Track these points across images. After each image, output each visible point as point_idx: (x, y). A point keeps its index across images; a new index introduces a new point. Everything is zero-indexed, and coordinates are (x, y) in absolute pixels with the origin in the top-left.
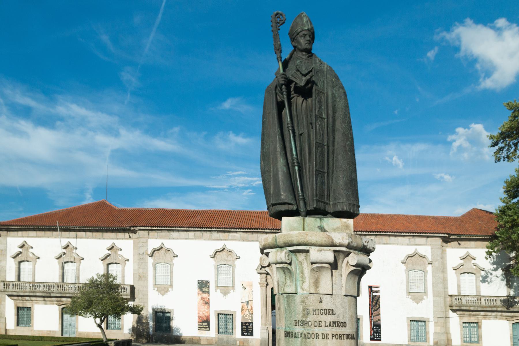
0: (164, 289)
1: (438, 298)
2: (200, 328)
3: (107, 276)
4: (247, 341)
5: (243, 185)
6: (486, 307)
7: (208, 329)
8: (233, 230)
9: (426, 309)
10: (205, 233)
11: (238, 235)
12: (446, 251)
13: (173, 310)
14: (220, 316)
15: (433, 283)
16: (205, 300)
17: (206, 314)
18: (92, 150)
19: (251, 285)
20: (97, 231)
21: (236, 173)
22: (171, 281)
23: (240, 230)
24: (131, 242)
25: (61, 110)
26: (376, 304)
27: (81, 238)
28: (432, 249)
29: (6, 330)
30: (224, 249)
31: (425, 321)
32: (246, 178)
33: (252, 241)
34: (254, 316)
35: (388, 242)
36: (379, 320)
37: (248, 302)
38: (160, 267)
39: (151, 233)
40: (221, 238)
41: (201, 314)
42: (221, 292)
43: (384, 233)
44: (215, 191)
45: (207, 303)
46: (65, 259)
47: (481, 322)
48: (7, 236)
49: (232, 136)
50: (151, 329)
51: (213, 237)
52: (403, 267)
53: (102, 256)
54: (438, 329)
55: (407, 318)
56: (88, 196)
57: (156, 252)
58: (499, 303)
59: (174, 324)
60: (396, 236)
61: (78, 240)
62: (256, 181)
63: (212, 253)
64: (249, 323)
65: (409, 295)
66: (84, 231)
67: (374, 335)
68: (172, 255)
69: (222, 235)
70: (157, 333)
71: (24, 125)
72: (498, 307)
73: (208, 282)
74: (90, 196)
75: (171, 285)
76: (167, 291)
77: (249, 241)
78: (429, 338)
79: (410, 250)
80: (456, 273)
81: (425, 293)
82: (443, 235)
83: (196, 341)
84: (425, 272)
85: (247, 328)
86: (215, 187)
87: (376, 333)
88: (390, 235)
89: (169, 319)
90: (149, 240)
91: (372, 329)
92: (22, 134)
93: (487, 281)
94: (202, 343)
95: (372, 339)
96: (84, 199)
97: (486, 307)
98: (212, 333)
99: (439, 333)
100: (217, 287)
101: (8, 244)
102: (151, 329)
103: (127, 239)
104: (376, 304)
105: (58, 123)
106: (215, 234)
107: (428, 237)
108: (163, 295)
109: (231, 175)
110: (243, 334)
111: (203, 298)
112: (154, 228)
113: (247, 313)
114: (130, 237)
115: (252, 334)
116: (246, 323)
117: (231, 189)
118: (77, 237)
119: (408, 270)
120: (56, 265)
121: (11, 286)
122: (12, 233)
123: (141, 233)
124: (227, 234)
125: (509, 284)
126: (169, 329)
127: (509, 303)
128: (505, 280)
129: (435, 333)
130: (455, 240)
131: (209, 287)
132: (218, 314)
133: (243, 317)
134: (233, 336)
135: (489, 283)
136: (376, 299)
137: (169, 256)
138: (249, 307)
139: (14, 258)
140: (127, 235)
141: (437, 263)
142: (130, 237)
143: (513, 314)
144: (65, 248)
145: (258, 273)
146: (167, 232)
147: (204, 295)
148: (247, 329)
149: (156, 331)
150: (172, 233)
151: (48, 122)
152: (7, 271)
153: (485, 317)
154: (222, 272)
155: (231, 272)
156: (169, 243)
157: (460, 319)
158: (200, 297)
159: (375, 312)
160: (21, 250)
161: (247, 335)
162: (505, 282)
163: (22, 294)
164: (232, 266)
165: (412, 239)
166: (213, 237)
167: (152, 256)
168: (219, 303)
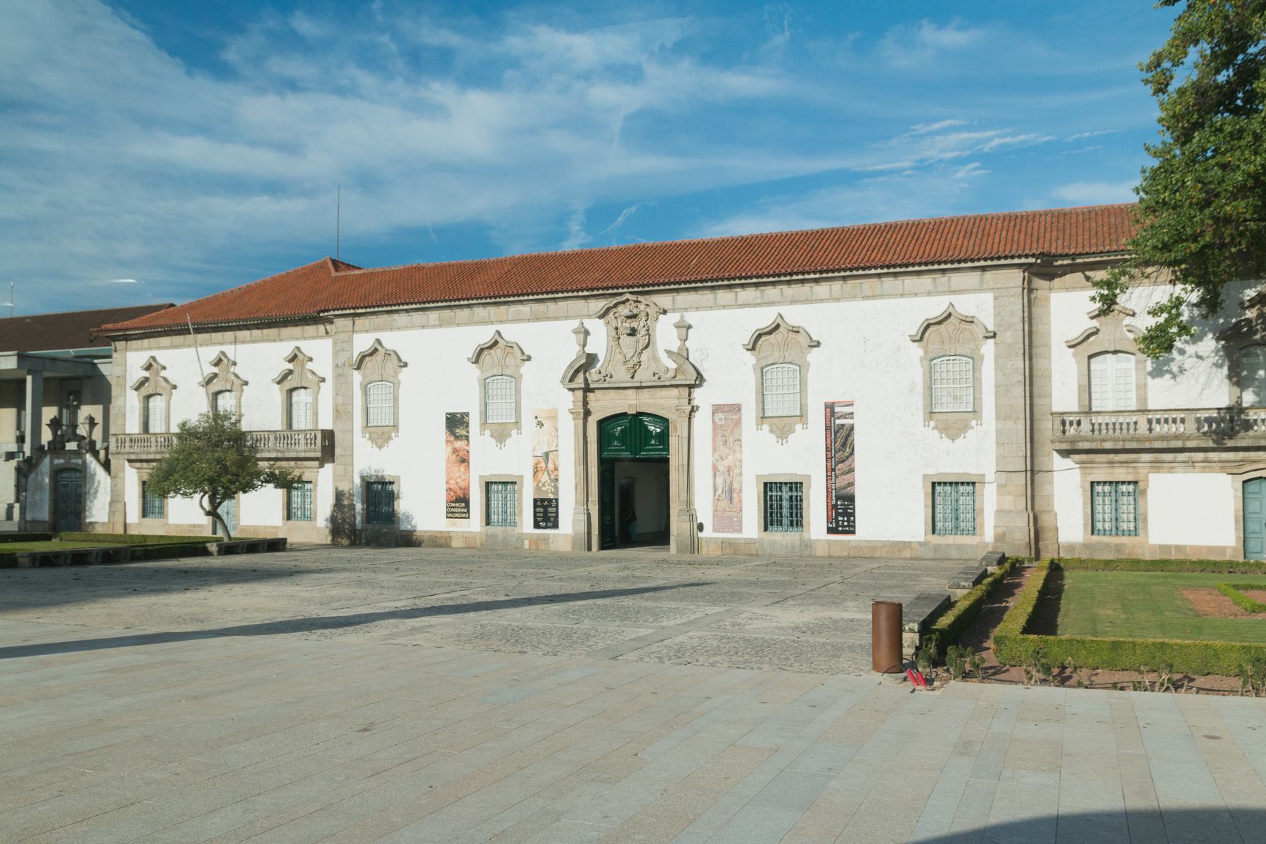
0: (382, 435)
1: (1010, 424)
2: (450, 515)
3: (217, 416)
4: (546, 539)
5: (956, 154)
6: (1150, 440)
7: (466, 515)
8: (765, 280)
9: (980, 452)
10: (459, 312)
11: (525, 309)
12: (1048, 299)
13: (399, 477)
14: (1099, 489)
15: (997, 386)
16: (461, 454)
17: (463, 484)
18: (582, 123)
19: (554, 417)
20: (270, 325)
21: (936, 126)
22: (396, 418)
23: (720, 283)
24: (328, 343)
25: (514, 43)
26: (844, 445)
27: (243, 342)
28: (996, 298)
29: (125, 525)
30: (950, 315)
31: (974, 483)
32: (964, 135)
33: (557, 318)
34: (561, 484)
35: (877, 293)
36: (852, 484)
37: (547, 454)
38: (772, 374)
39: (359, 321)
40: (493, 319)
41: (452, 484)
42: (492, 436)
43: (861, 272)
44: (880, 179)
45: (464, 461)
46: (289, 384)
47: (1146, 480)
48: (126, 350)
49: (929, 34)
50: (359, 519)
51: (476, 319)
52: (917, 351)
53: (277, 374)
54: (1009, 502)
55: (925, 476)
56: (575, 227)
57: (486, 352)
58: (1191, 427)
59: (402, 506)
60: (895, 275)
61: (239, 346)
62: (991, 139)
63: (747, 338)
64: (550, 500)
65: (931, 419)
66: (246, 327)
67: (837, 521)
68: (806, 342)
69: (493, 310)
70: (370, 526)
71: (439, 91)
72: (1188, 438)
73: (467, 414)
74: (578, 228)
75: (395, 427)
76: (389, 438)
77: (549, 319)
78: (982, 525)
79: (934, 306)
80: (1075, 355)
81: (976, 412)
82: (1023, 260)
83: (442, 541)
84: (976, 360)
85: (546, 512)
86: (878, 167)
87: (842, 515)
88: (879, 276)
89: (391, 497)
90: (356, 336)
91: (832, 508)
92: (437, 111)
93: (1170, 372)
94: (454, 544)
95: (831, 531)
96: (564, 236)
97: (1150, 440)
98: (474, 524)
99: (1010, 511)
100: (484, 424)
101: (128, 364)
102: (359, 519)
103: (322, 337)
104: (844, 445)
105: (509, 74)
106: (480, 312)
107: (984, 269)
108: (380, 448)
109: (923, 131)
110: (537, 525)
111: (455, 451)
112: (360, 311)
113: (545, 478)
114: (327, 333)
115: (556, 526)
116: (543, 500)
117: (924, 167)
118: (235, 342)
119: (930, 360)
120: (276, 395)
121: (128, 444)
122: (133, 344)
123: (340, 322)
124: (503, 308)
125: (1238, 375)
126: (391, 517)
127: (1227, 430)
128: (1227, 363)
129: (999, 512)
130: (1073, 268)
131: (467, 426)
132: (933, 484)
133: (537, 488)
134: (517, 530)
135: (1174, 377)
136: (843, 433)
137: (392, 364)
138: (551, 466)
139: (278, 383)
140: (321, 328)
141: (1009, 333)
142: (327, 333)
143: (1241, 455)
144: (291, 361)
145: (570, 389)
146: (386, 316)
147: (459, 444)
148: (546, 513)
149: (368, 522)
150: (396, 316)
151: (484, 76)
152: (128, 416)
153: (1157, 466)
154: (780, 382)
155: (513, 391)
156: (391, 340)
157: (1084, 474)
158: (449, 449)
159: (840, 466)
160: (291, 366)
161: (546, 527)
162: (1225, 370)
163: (144, 457)
164: (517, 378)
165: (942, 279)
166: (476, 319)
167: (358, 368)
168: (488, 456)
